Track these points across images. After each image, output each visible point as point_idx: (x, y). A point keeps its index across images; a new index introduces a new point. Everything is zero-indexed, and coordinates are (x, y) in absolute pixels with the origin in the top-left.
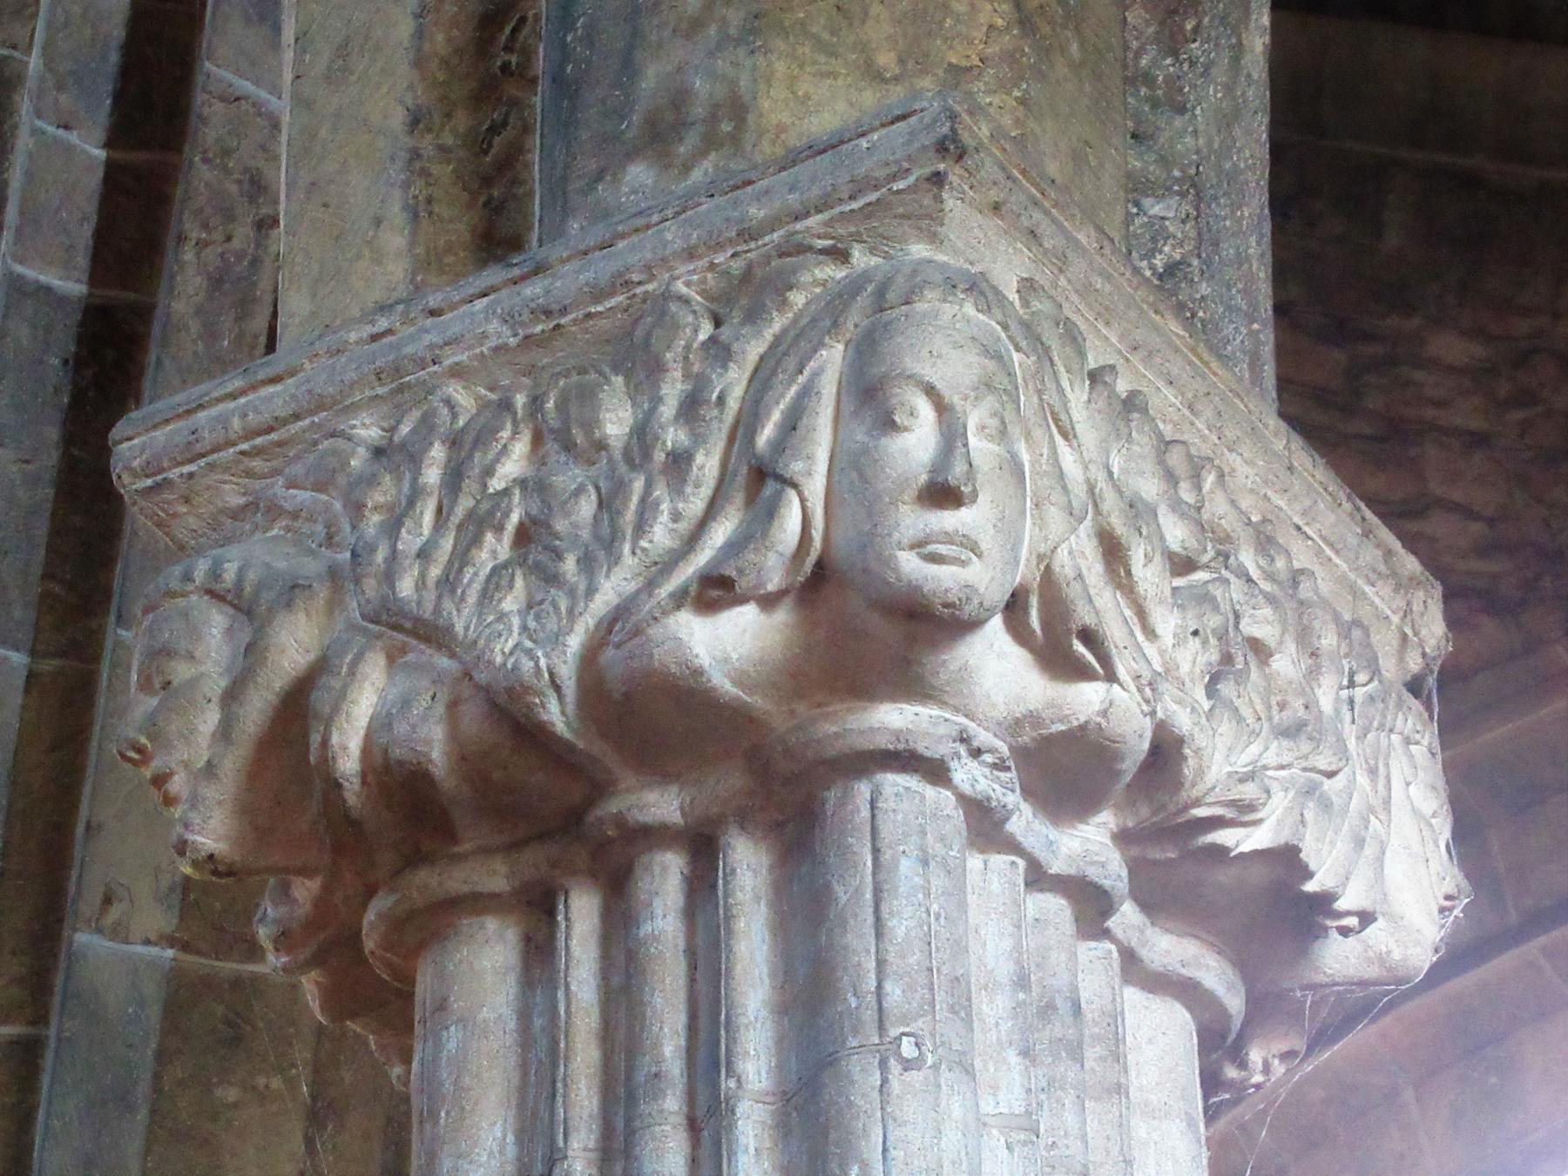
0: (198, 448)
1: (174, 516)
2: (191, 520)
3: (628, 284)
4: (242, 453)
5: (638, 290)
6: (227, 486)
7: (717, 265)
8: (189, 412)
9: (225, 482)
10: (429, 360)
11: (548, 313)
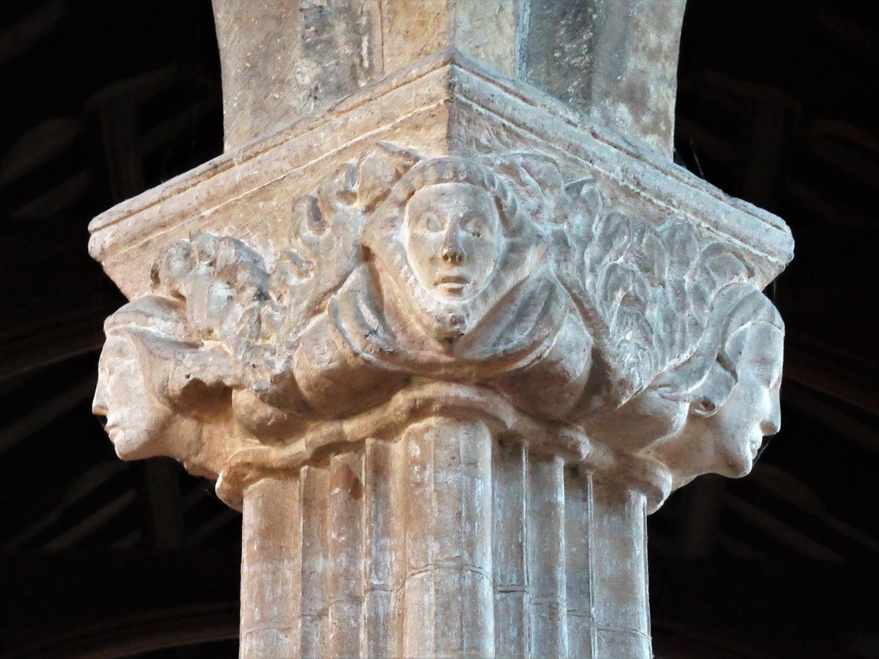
0: (490, 105)
1: (460, 123)
2: (463, 130)
3: (670, 202)
4: (504, 125)
5: (672, 208)
6: (486, 131)
7: (701, 227)
8: (488, 79)
9: (488, 129)
10: (590, 159)
11: (638, 184)
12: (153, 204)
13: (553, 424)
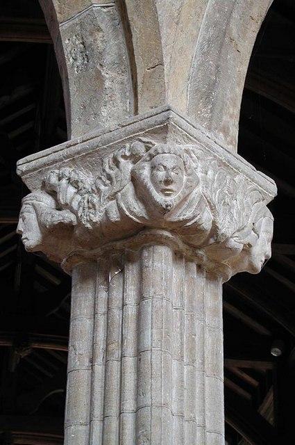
12: (43, 157)
13: (195, 248)
